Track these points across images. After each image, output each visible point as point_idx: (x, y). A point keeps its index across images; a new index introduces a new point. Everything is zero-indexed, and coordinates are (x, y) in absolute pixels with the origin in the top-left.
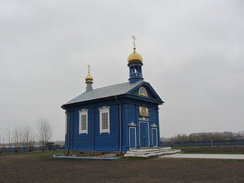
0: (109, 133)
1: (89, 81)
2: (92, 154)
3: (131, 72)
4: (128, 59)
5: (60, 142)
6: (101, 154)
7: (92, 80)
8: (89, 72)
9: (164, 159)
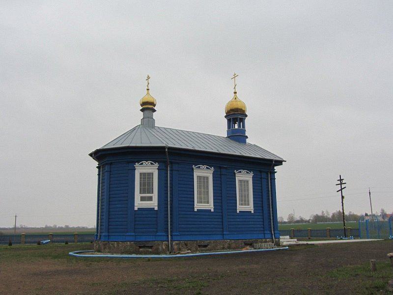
0: (253, 212)
1: (148, 107)
2: (226, 246)
3: (229, 127)
4: (226, 108)
5: (22, 227)
6: (243, 244)
7: (154, 105)
8: (148, 90)
9: (328, 245)
